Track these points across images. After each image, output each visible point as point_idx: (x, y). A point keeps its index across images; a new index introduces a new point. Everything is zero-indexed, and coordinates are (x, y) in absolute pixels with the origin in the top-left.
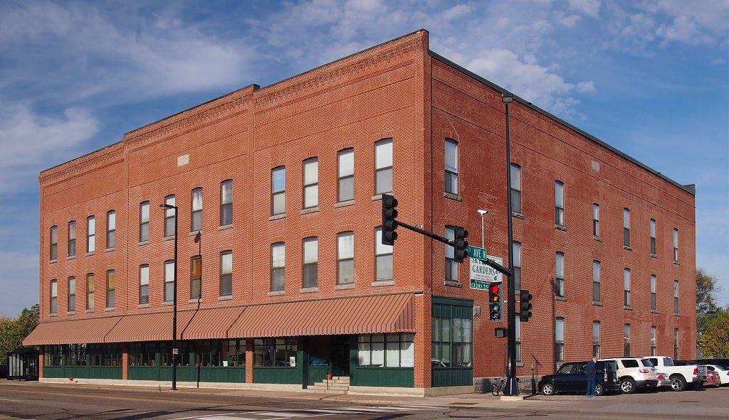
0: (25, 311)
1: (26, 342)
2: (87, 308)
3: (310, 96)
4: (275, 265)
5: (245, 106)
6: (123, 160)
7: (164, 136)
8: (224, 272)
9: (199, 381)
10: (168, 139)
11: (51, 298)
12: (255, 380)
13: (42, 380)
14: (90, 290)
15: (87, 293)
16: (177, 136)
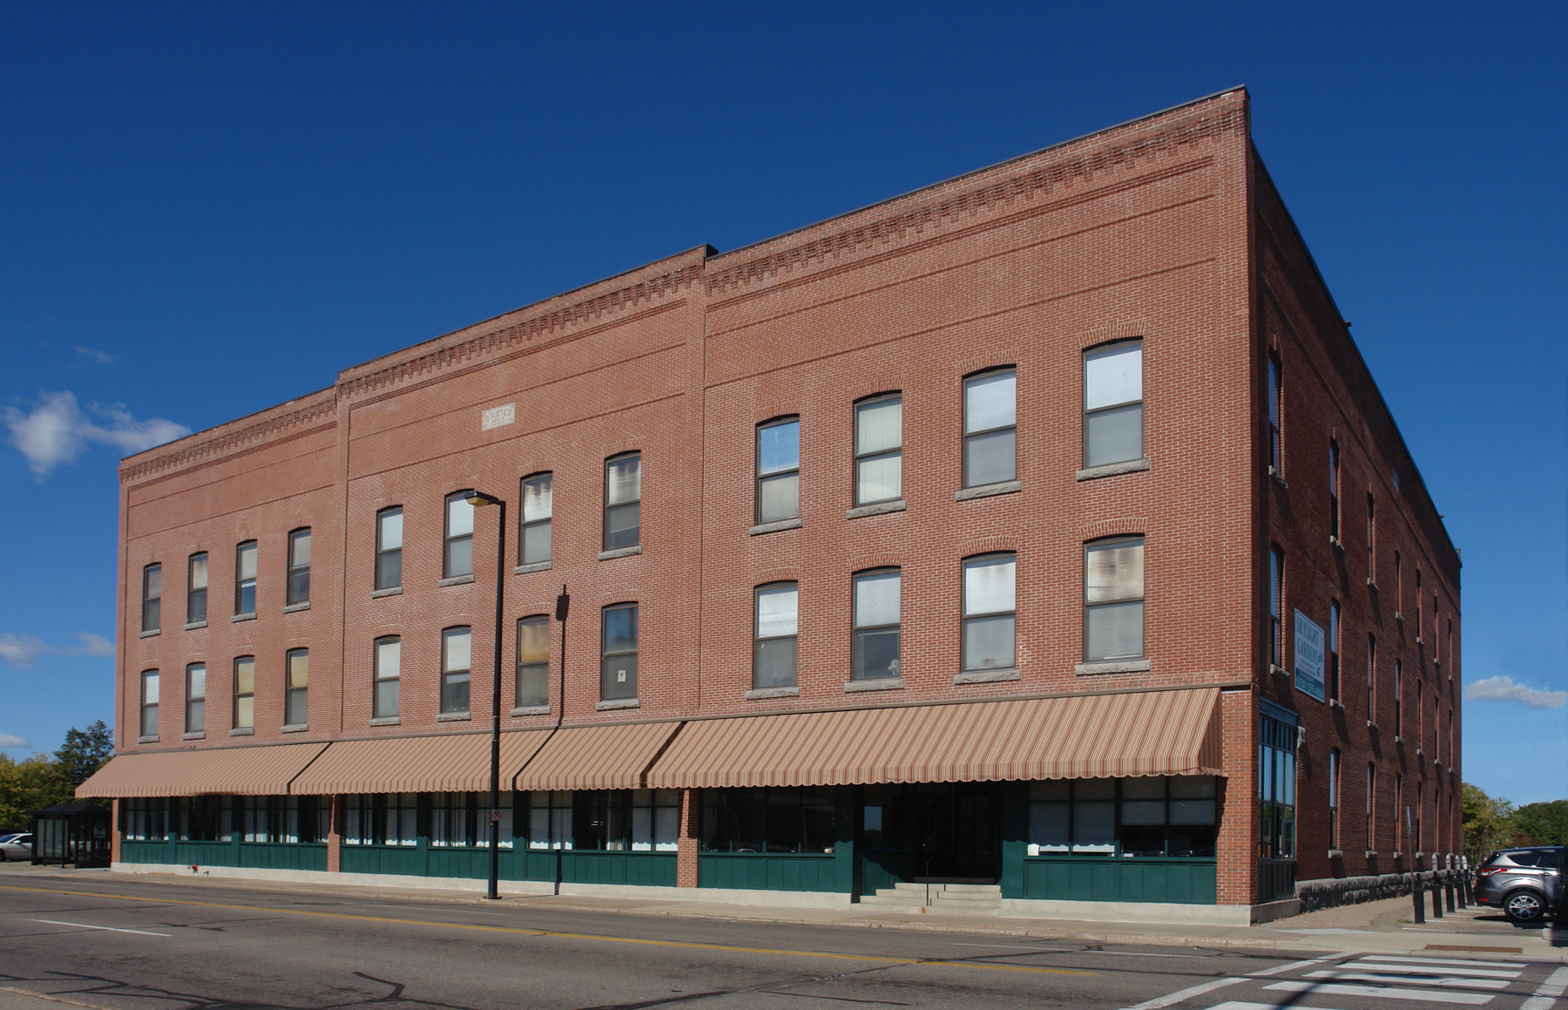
0: (73, 734)
1: (84, 791)
2: (235, 724)
3: (878, 259)
4: (764, 631)
5: (682, 292)
6: (333, 425)
7: (446, 369)
8: (863, 620)
9: (559, 880)
10: (458, 374)
11: (144, 707)
12: (704, 880)
13: (118, 867)
14: (242, 690)
15: (236, 697)
16: (480, 367)
